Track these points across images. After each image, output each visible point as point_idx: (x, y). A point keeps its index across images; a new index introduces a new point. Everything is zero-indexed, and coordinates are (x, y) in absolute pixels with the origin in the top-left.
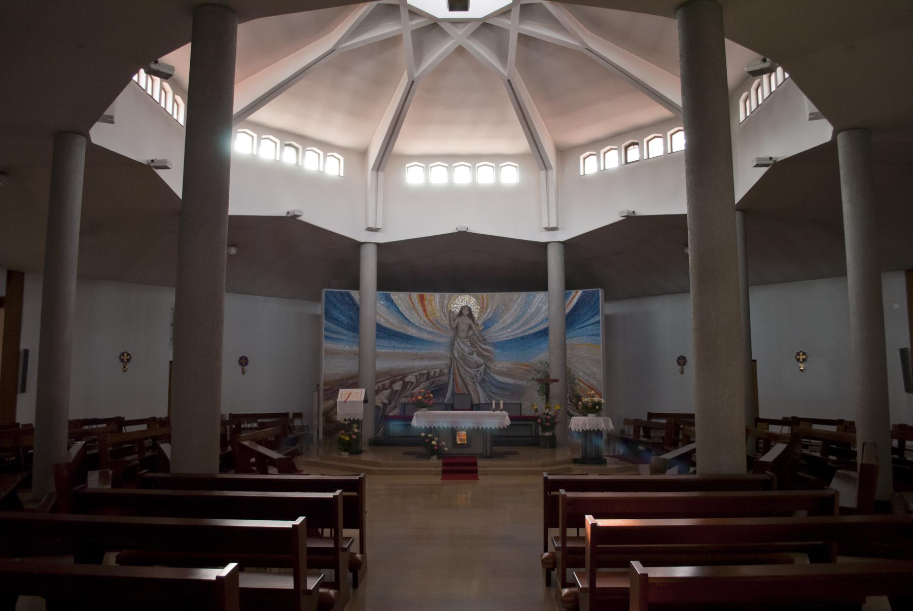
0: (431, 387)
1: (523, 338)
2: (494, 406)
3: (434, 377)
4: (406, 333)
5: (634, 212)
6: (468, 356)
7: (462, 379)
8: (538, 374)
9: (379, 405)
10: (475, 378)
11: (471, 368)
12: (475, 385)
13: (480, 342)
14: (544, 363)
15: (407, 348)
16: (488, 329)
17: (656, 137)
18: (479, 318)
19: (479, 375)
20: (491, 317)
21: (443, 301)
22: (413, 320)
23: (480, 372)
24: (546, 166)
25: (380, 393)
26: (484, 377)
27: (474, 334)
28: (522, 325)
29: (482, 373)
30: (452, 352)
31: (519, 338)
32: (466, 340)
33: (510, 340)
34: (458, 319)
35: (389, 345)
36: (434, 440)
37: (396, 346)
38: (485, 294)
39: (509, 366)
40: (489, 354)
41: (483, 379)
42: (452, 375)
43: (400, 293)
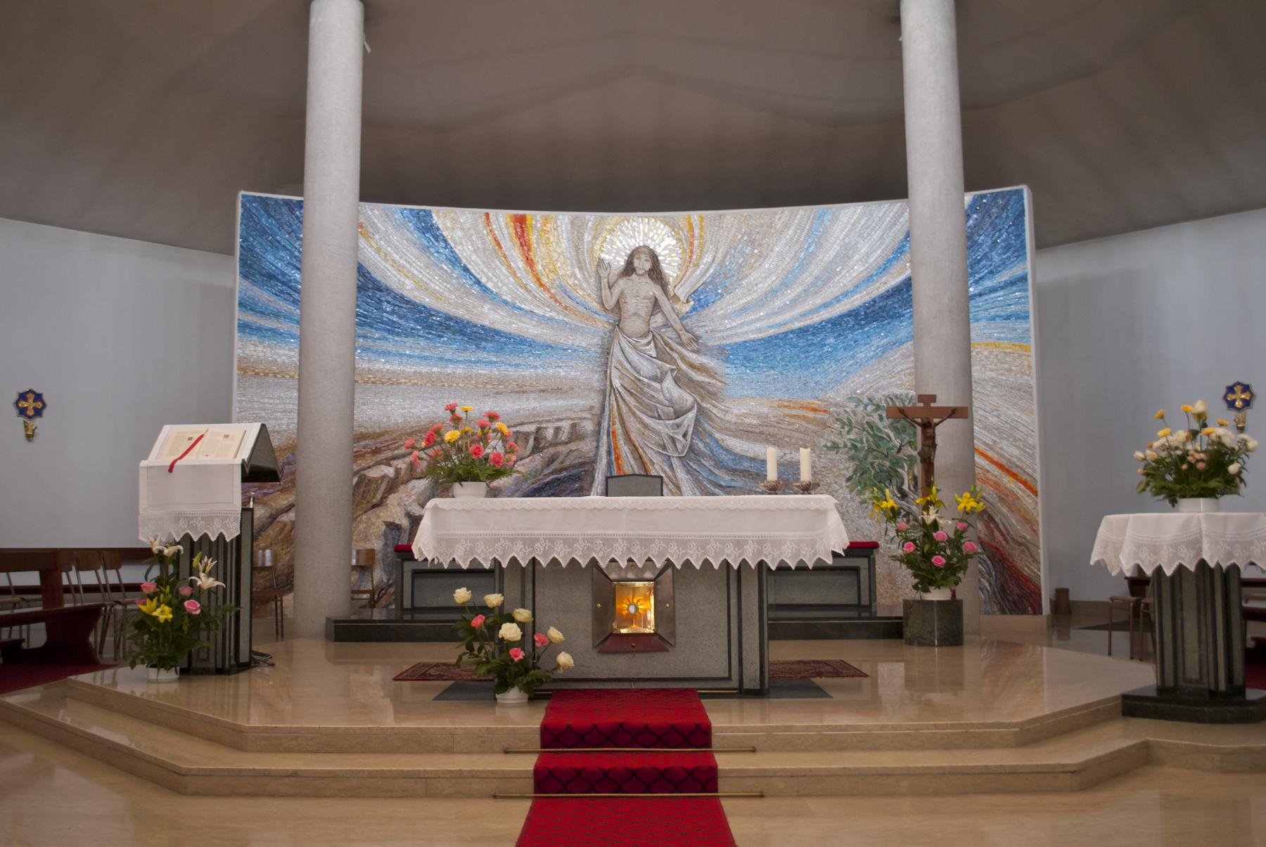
1: (803, 331)
4: (475, 320)
6: (649, 386)
8: (849, 432)
9: (397, 522)
10: (669, 445)
11: (659, 418)
12: (671, 466)
13: (682, 344)
14: (866, 401)
19: (680, 437)
23: (682, 430)
27: (667, 325)
31: (792, 332)
32: (644, 341)
34: (623, 283)
38: (695, 216)
40: (707, 380)
41: (692, 449)
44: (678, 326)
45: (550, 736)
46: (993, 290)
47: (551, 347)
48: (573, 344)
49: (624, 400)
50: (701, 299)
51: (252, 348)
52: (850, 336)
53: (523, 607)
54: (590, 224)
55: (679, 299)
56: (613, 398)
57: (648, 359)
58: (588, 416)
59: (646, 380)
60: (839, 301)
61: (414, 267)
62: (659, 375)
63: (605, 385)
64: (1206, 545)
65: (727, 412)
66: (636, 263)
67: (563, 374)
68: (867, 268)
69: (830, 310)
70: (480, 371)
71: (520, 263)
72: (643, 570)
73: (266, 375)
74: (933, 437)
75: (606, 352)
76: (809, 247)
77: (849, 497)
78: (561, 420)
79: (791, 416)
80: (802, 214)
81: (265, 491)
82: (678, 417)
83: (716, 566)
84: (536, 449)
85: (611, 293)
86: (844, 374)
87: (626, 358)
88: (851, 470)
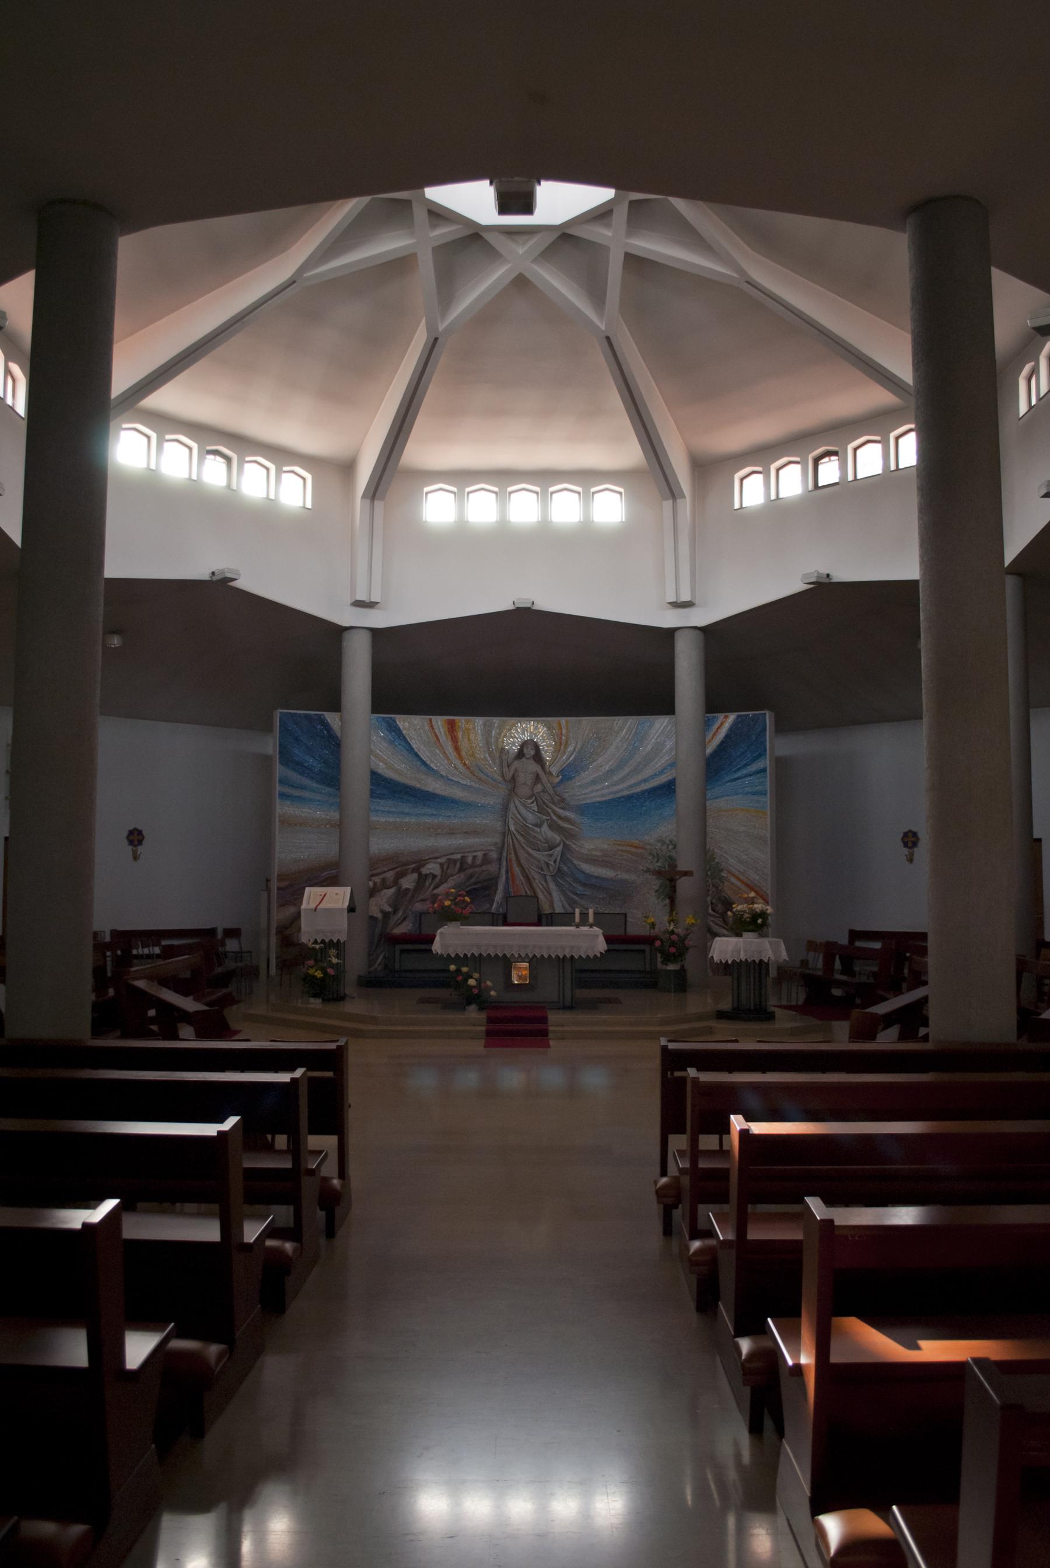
1: (630, 797)
3: (473, 866)
4: (423, 788)
5: (828, 575)
6: (533, 830)
8: (657, 861)
9: (375, 916)
10: (545, 868)
11: (539, 850)
12: (546, 881)
13: (554, 803)
14: (668, 842)
15: (424, 815)
17: (868, 442)
18: (553, 761)
19: (552, 863)
21: (489, 733)
23: (553, 859)
24: (672, 492)
27: (544, 791)
31: (623, 797)
32: (530, 801)
34: (517, 764)
36: (471, 977)
37: (407, 810)
38: (563, 720)
40: (569, 826)
41: (559, 870)
44: (551, 792)
45: (490, 1020)
46: (746, 776)
47: (470, 804)
48: (484, 803)
49: (517, 838)
50: (567, 774)
51: (287, 808)
52: (659, 801)
53: (476, 972)
54: (496, 725)
55: (552, 775)
56: (510, 837)
57: (532, 813)
58: (494, 849)
59: (530, 826)
60: (653, 778)
61: (385, 755)
62: (539, 823)
63: (505, 829)
64: (742, 952)
65: (582, 847)
66: (525, 751)
67: (478, 822)
68: (671, 758)
69: (647, 784)
70: (426, 821)
71: (450, 749)
72: (525, 958)
73: (296, 825)
74: (675, 887)
75: (506, 808)
76: (635, 743)
77: (656, 902)
78: (478, 851)
79: (622, 851)
80: (631, 721)
81: (295, 897)
82: (551, 850)
83: (554, 957)
84: (461, 870)
85: (509, 770)
86: (655, 825)
87: (518, 812)
88: (658, 885)
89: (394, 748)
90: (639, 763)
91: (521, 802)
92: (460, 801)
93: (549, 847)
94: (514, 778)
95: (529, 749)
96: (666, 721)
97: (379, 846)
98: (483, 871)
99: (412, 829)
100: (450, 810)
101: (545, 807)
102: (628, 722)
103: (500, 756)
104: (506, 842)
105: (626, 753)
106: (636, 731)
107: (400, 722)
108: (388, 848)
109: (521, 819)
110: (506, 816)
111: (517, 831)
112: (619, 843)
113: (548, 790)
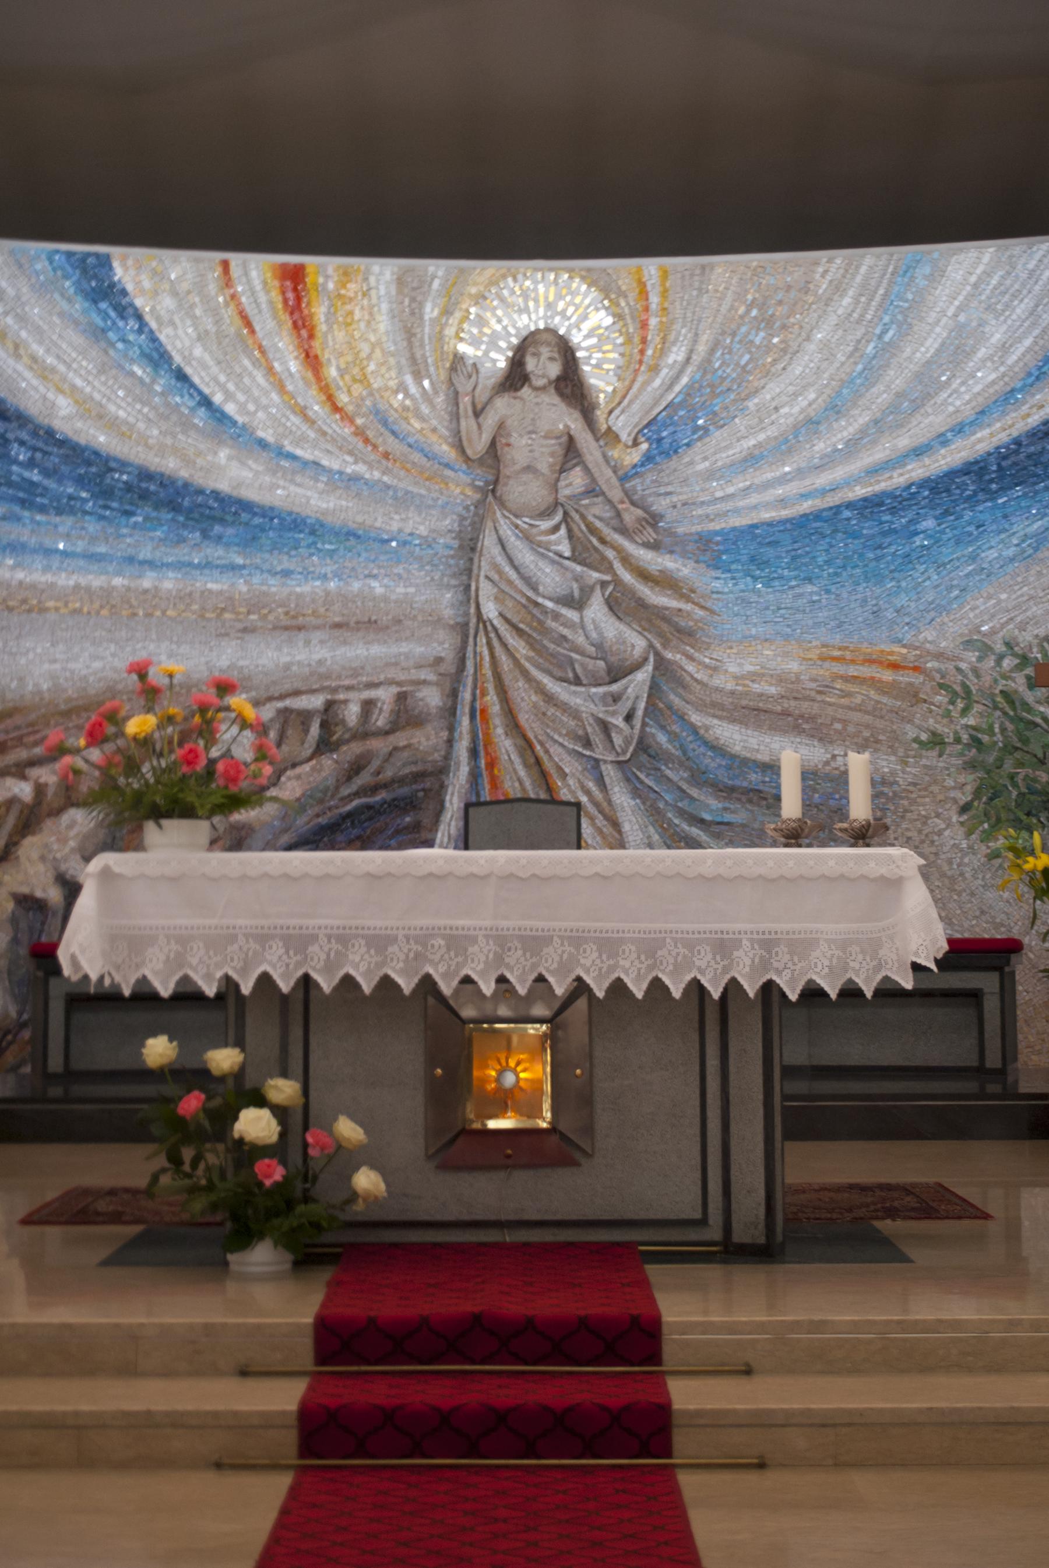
0: (345, 791)
1: (870, 506)
2: (791, 806)
3: (363, 734)
4: (200, 480)
6: (556, 616)
7: (526, 746)
8: (965, 712)
9: (39, 894)
10: (597, 738)
11: (577, 681)
12: (601, 782)
13: (623, 531)
14: (1000, 648)
15: (207, 565)
16: (673, 463)
18: (619, 399)
19: (619, 721)
20: (689, 392)
21: (416, 312)
22: (242, 408)
23: (624, 707)
25: (49, 824)
26: (652, 730)
27: (593, 491)
28: (863, 432)
29: (640, 713)
30: (468, 587)
31: (849, 505)
32: (546, 525)
33: (801, 524)
34: (503, 405)
35: (102, 549)
36: (259, 1100)
37: (145, 553)
38: (651, 267)
39: (794, 666)
40: (674, 604)
41: (643, 746)
42: (465, 722)
43: (166, 255)
52: (968, 515)
53: (285, 1074)
54: (436, 284)
55: (617, 438)
56: (482, 640)
57: (553, 562)
58: (432, 677)
59: (549, 604)
60: (945, 443)
63: (467, 614)
68: (1004, 375)
72: (530, 998)
76: (884, 332)
77: (964, 845)
79: (846, 679)
82: (614, 681)
83: (677, 993)
85: (479, 426)
88: (969, 788)
89: (106, 352)
90: (898, 395)
91: (517, 526)
92: (322, 525)
93: (609, 671)
94: (494, 452)
95: (543, 358)
96: (986, 258)
97: (57, 666)
98: (396, 749)
99: (164, 613)
100: (287, 553)
101: (595, 541)
102: (858, 267)
103: (451, 382)
104: (470, 654)
105: (856, 363)
106: (886, 295)
107: (126, 269)
108: (84, 672)
109: (518, 582)
110: (469, 571)
111: (507, 621)
112: (836, 653)
113: (604, 488)
